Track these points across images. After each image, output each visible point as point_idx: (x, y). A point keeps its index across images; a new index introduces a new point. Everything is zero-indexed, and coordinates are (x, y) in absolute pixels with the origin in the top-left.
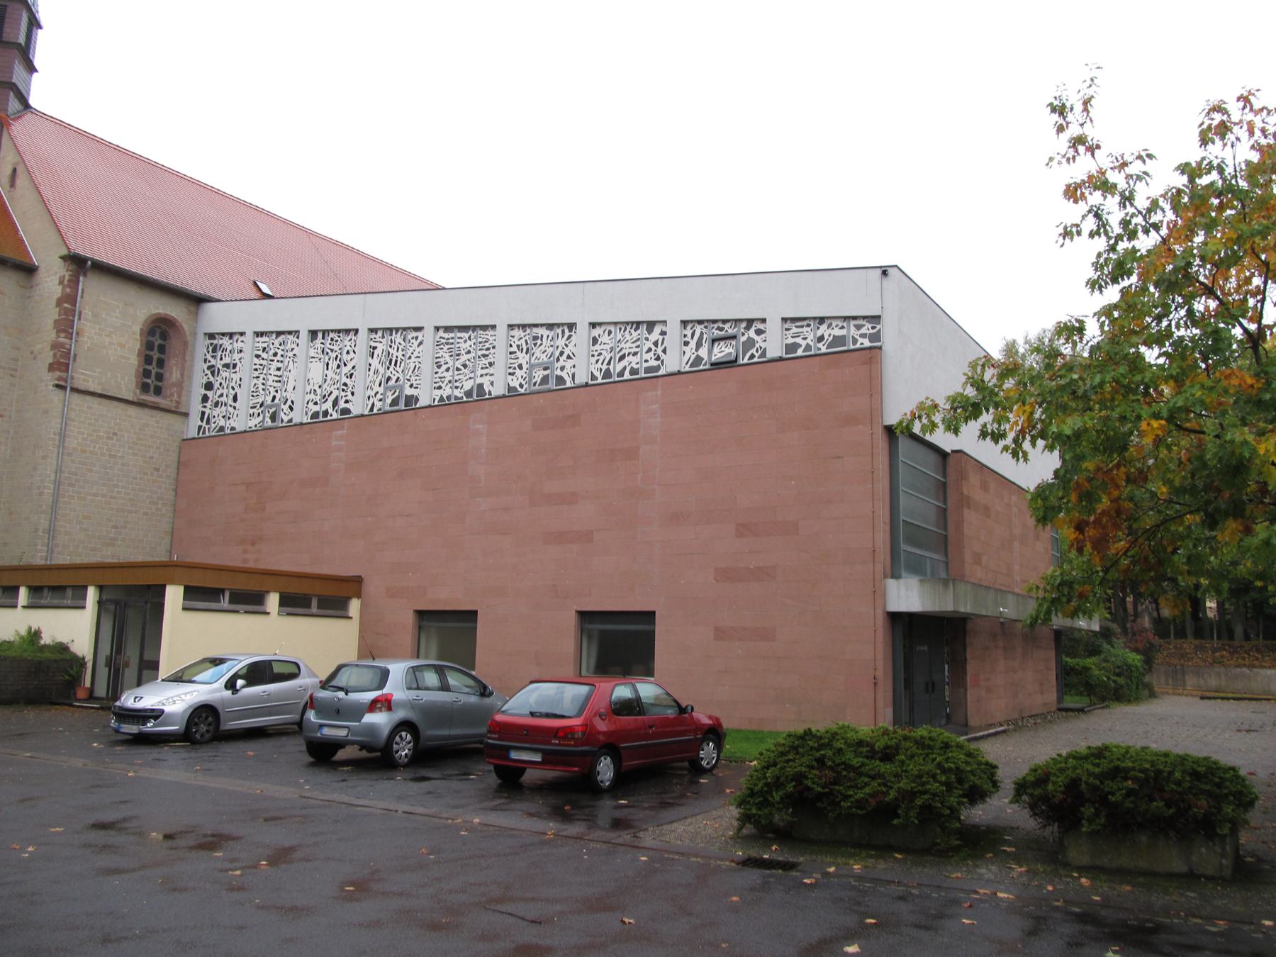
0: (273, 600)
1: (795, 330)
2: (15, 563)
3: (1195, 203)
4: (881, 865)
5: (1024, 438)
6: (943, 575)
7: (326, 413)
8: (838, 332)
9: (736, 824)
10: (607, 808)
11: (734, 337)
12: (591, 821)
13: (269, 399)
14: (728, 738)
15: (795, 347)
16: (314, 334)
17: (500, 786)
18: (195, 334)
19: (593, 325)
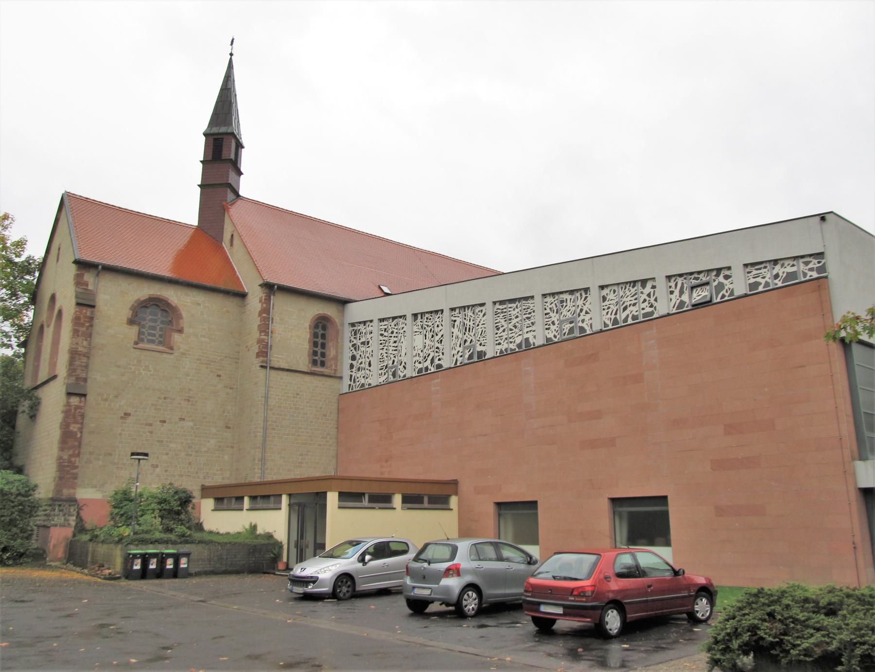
0: (397, 499)
1: (755, 272)
2: (243, 482)
7: (427, 369)
8: (790, 270)
11: (707, 284)
13: (391, 362)
15: (757, 284)
16: (415, 316)
18: (343, 325)
19: (602, 287)
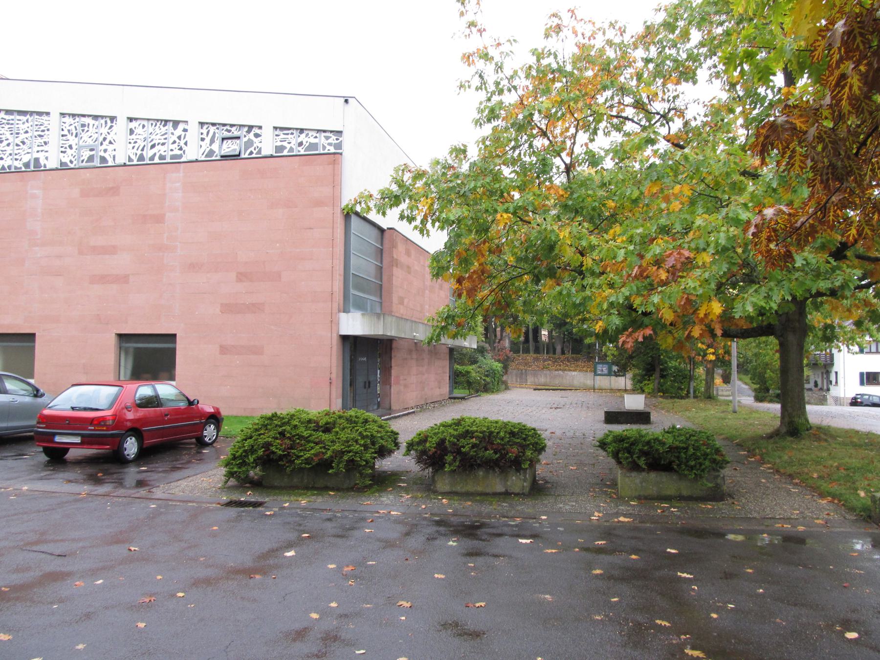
1: (282, 136)
3: (543, 77)
4: (320, 499)
5: (427, 221)
6: (378, 311)
8: (313, 140)
9: (223, 478)
10: (132, 473)
11: (238, 138)
12: (120, 483)
14: (224, 423)
15: (282, 148)
17: (49, 462)
19: (131, 120)
